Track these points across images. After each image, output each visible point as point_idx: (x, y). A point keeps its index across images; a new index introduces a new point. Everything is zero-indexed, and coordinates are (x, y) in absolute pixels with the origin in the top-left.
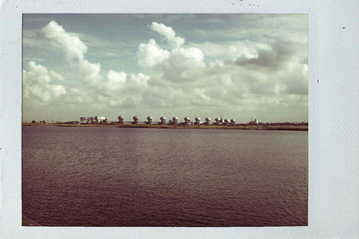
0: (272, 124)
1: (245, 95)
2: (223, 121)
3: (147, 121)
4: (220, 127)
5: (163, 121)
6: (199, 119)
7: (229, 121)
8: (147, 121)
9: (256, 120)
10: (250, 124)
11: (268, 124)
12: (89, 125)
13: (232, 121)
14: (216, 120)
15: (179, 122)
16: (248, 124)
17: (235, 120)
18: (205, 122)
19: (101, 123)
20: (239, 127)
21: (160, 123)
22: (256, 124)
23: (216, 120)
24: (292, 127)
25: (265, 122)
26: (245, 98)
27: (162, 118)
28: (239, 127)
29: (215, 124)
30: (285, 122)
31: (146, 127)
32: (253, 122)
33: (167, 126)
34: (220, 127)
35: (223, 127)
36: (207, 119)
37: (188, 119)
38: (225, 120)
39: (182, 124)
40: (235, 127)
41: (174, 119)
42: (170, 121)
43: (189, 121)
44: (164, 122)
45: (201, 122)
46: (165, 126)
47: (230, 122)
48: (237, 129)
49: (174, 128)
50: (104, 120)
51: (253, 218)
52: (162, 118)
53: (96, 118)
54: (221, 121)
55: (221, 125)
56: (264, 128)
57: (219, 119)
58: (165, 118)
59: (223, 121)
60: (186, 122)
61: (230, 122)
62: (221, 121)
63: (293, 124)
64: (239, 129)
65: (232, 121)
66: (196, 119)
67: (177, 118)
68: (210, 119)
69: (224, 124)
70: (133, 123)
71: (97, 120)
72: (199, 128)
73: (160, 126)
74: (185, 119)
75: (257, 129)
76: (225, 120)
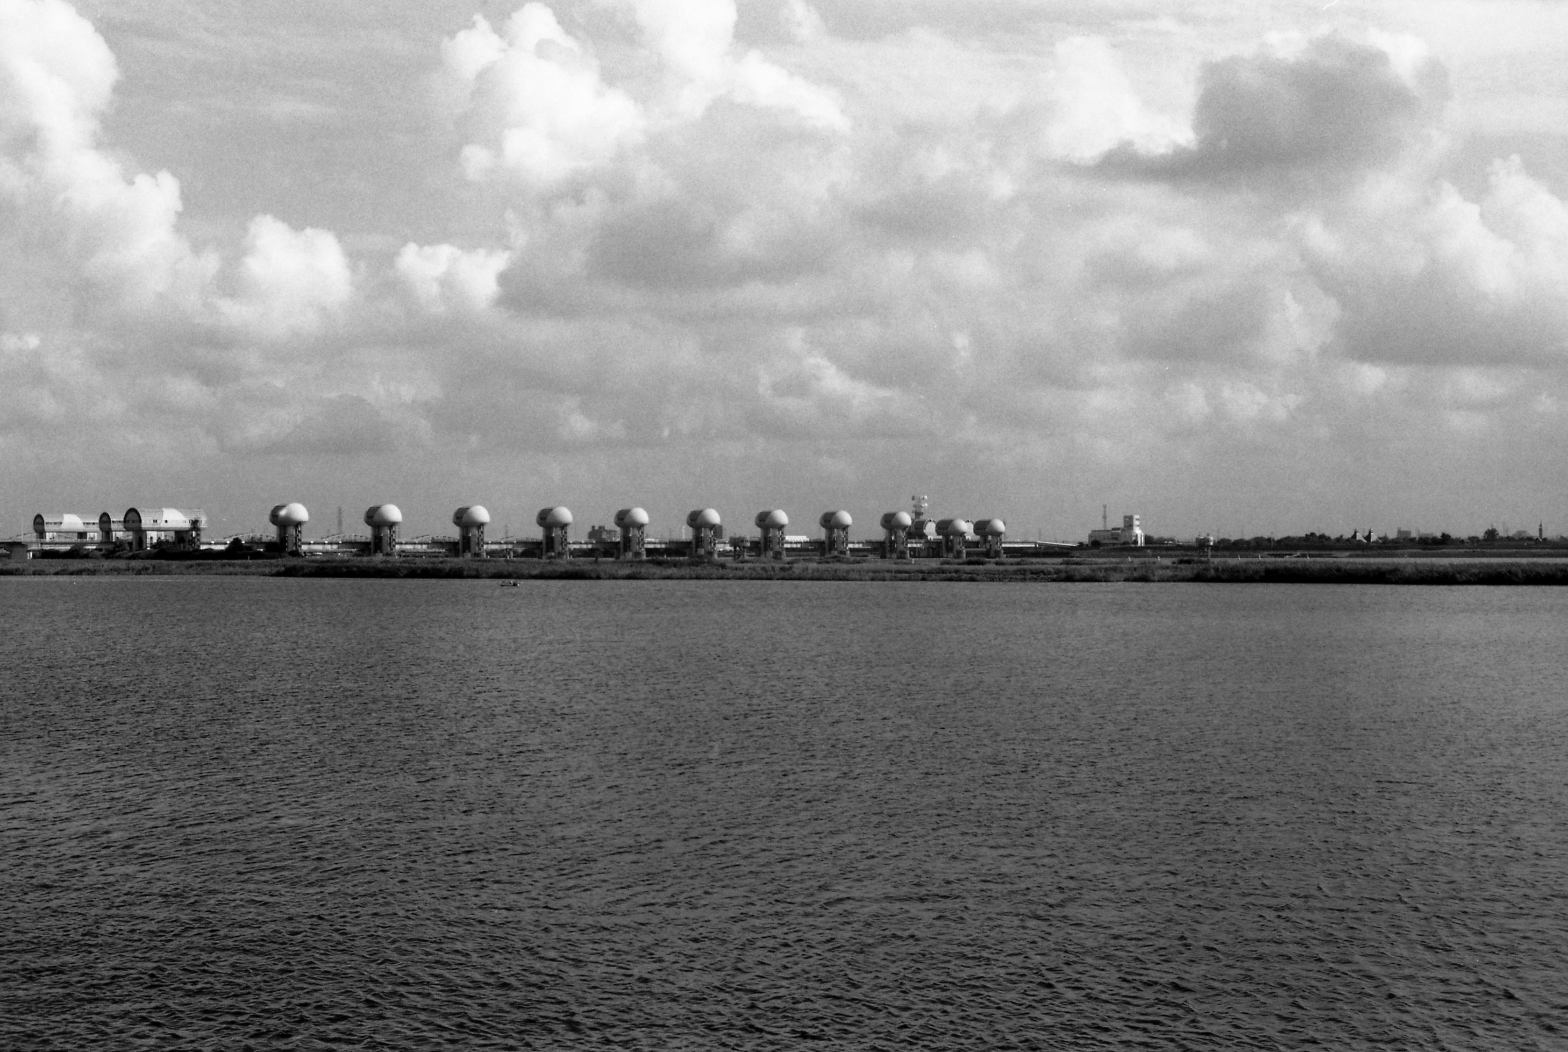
0: (1226, 547)
1: (1101, 371)
2: (931, 531)
3: (454, 533)
4: (914, 564)
5: (556, 533)
6: (782, 517)
7: (966, 527)
8: (454, 533)
9: (1129, 524)
10: (1095, 544)
11: (1202, 545)
12: (88, 564)
13: (982, 527)
14: (890, 522)
15: (653, 539)
16: (1081, 546)
17: (1000, 525)
18: (821, 534)
19: (163, 551)
20: (1037, 563)
21: (532, 549)
22: (1127, 547)
23: (890, 522)
24: (1343, 560)
25: (1186, 535)
26: (1095, 384)
27: (546, 519)
28: (1037, 563)
29: (880, 549)
30: (1299, 531)
31: (457, 574)
32: (1114, 534)
33: (583, 564)
34: (914, 564)
35: (934, 563)
36: (829, 521)
37: (714, 516)
38: (944, 527)
39: (677, 549)
40: (1010, 564)
41: (624, 519)
42: (595, 533)
43: (717, 530)
44: (564, 541)
45: (794, 539)
46: (565, 563)
47: (970, 535)
48: (1023, 576)
49: (629, 577)
50: (180, 534)
51: (1089, 1042)
52: (546, 519)
53: (132, 518)
54: (917, 531)
55: (915, 553)
56: (1187, 570)
57: (906, 519)
58: (565, 514)
59: (931, 531)
60: (699, 540)
61: (970, 535)
62: (917, 531)
63: (1350, 545)
64: (1039, 576)
65: (982, 527)
66: (765, 521)
67: (642, 515)
68: (846, 518)
69: (934, 550)
70: (364, 548)
71: (140, 533)
72: (786, 575)
73: (538, 564)
74: (696, 520)
75: (1144, 579)
76: (944, 527)
